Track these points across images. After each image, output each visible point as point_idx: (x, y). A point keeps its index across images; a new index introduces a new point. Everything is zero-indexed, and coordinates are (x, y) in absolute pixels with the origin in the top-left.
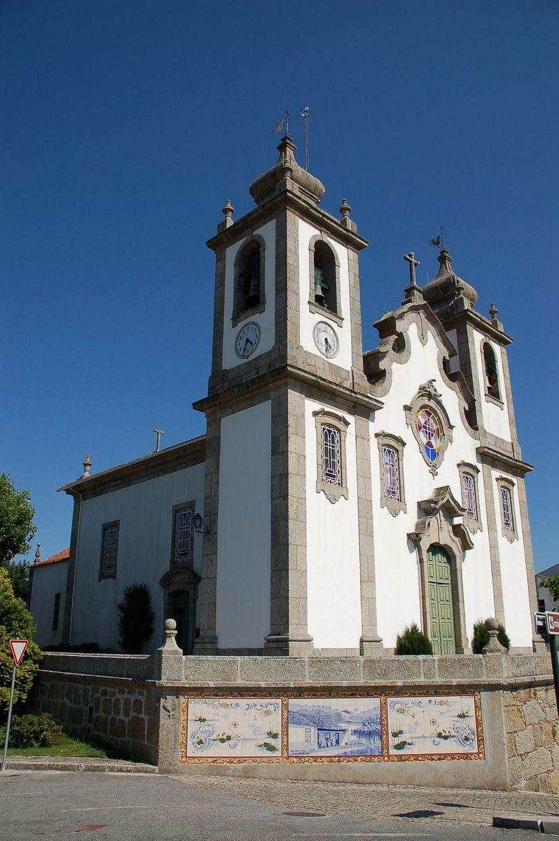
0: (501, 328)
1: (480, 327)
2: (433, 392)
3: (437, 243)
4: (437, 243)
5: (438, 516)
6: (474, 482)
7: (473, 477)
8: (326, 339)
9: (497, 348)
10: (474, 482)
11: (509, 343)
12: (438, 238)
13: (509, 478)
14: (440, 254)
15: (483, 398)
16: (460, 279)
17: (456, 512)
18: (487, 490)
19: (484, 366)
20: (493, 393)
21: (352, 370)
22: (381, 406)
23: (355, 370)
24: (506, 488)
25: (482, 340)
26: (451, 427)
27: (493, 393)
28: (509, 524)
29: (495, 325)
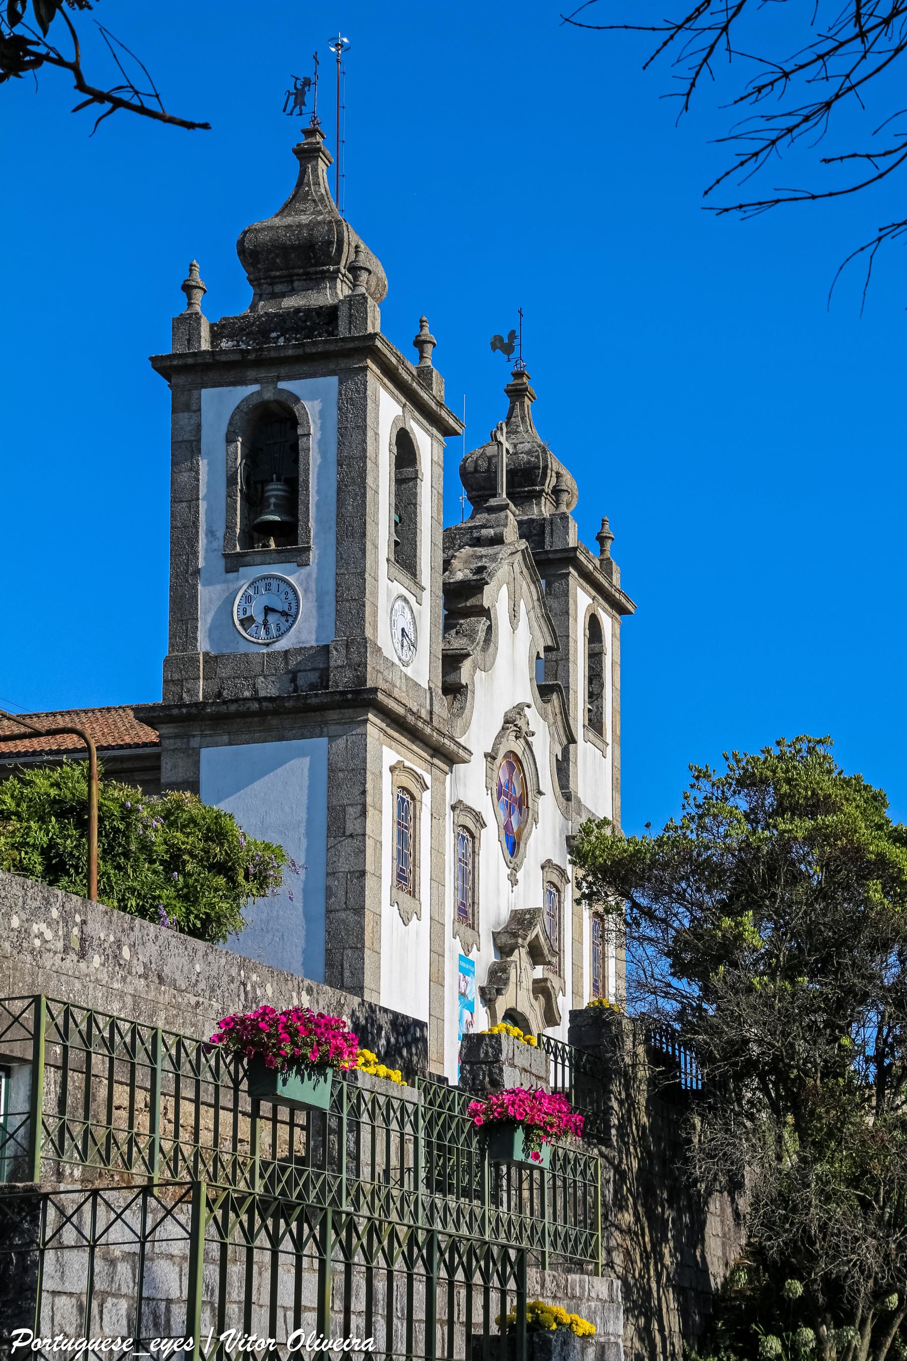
0: (438, 387)
1: (587, 577)
2: (524, 728)
3: (508, 349)
4: (508, 349)
5: (587, 1000)
6: (559, 902)
7: (558, 890)
8: (403, 630)
9: (607, 622)
10: (559, 902)
11: (629, 612)
12: (512, 335)
13: (419, 771)
14: (498, 351)
15: (383, 567)
16: (564, 471)
17: (542, 955)
18: (576, 919)
19: (393, 496)
20: (595, 723)
21: (430, 688)
22: (467, 756)
23: (432, 686)
24: (555, 886)
25: (397, 418)
26: (540, 793)
27: (595, 723)
28: (405, 879)
29: (607, 569)
